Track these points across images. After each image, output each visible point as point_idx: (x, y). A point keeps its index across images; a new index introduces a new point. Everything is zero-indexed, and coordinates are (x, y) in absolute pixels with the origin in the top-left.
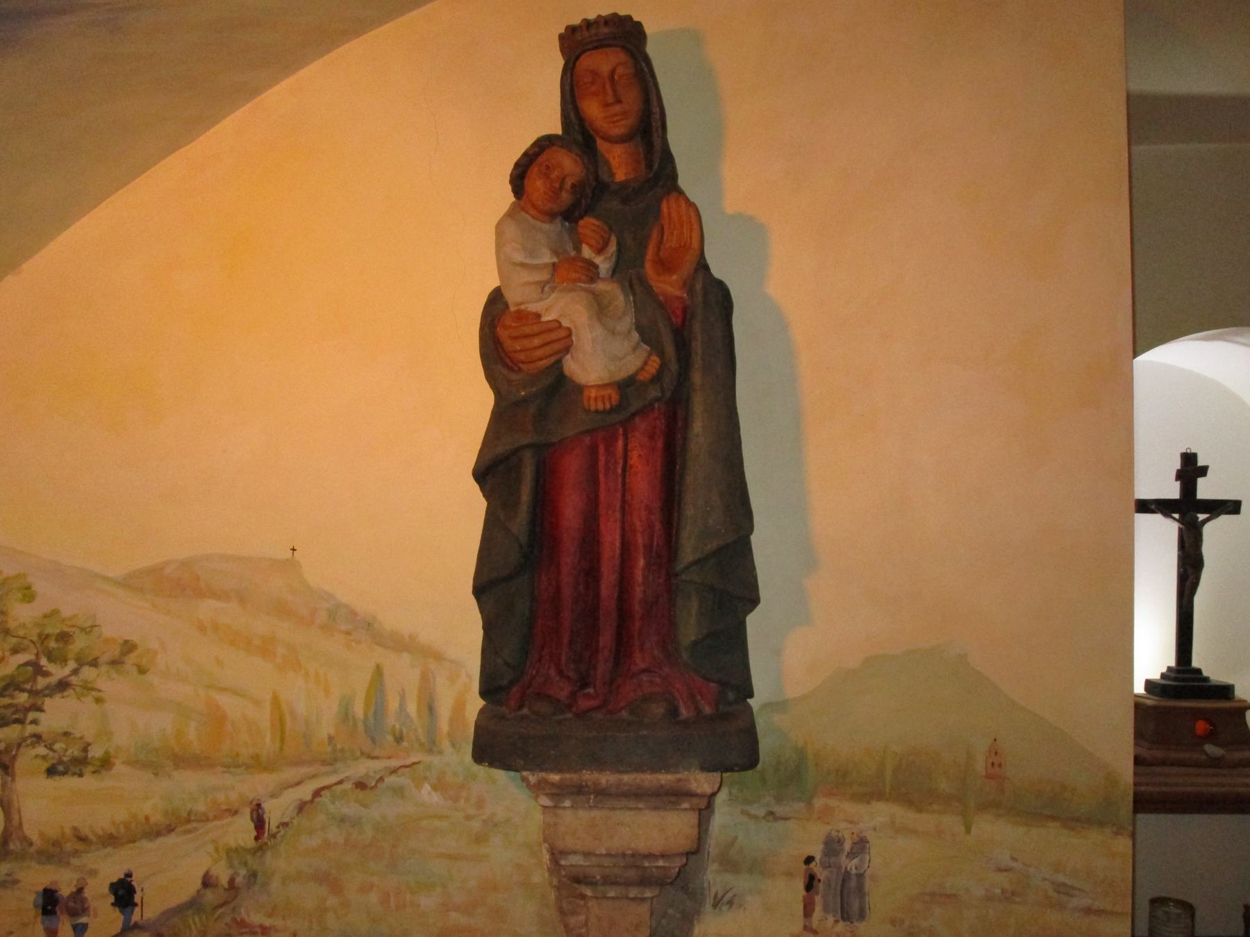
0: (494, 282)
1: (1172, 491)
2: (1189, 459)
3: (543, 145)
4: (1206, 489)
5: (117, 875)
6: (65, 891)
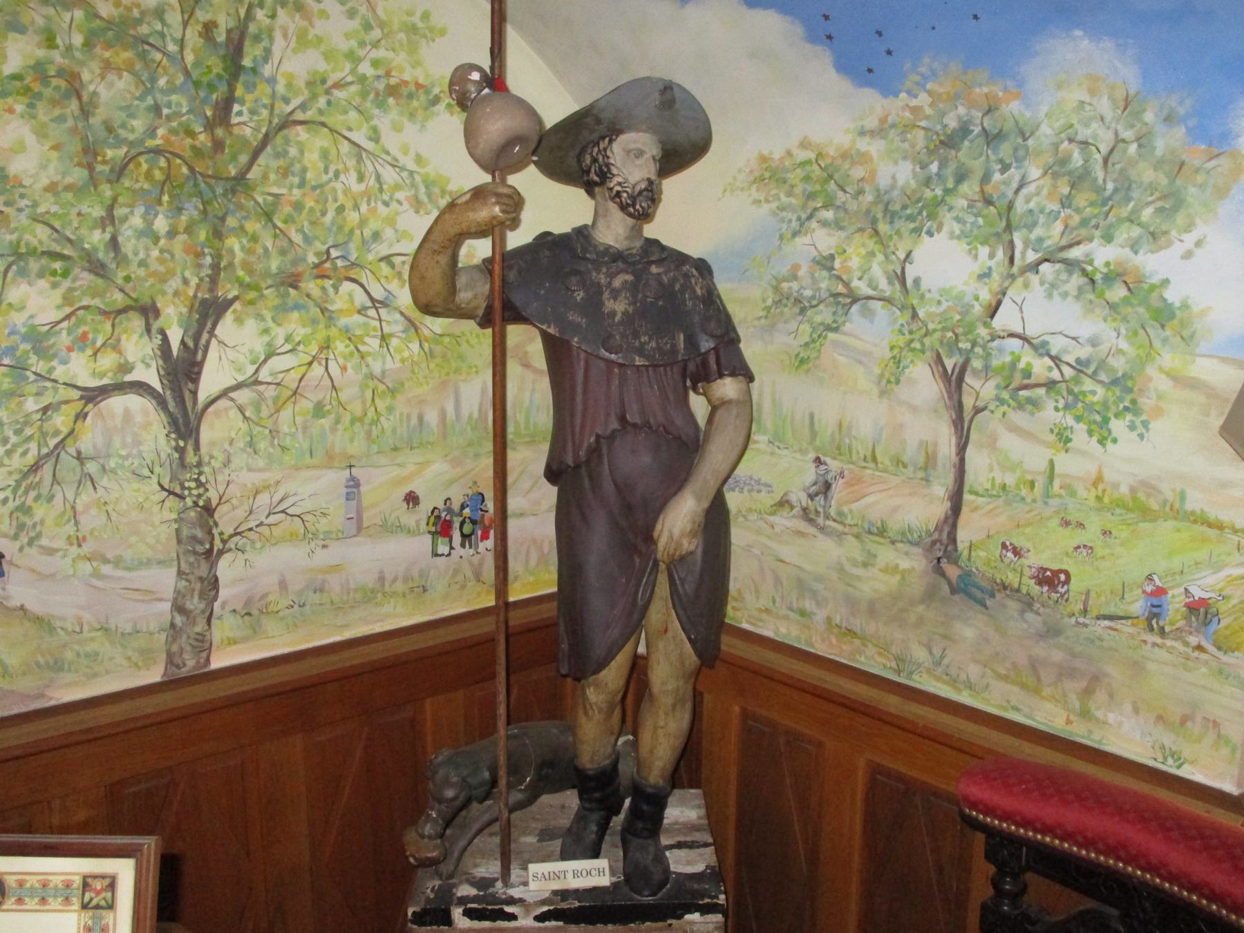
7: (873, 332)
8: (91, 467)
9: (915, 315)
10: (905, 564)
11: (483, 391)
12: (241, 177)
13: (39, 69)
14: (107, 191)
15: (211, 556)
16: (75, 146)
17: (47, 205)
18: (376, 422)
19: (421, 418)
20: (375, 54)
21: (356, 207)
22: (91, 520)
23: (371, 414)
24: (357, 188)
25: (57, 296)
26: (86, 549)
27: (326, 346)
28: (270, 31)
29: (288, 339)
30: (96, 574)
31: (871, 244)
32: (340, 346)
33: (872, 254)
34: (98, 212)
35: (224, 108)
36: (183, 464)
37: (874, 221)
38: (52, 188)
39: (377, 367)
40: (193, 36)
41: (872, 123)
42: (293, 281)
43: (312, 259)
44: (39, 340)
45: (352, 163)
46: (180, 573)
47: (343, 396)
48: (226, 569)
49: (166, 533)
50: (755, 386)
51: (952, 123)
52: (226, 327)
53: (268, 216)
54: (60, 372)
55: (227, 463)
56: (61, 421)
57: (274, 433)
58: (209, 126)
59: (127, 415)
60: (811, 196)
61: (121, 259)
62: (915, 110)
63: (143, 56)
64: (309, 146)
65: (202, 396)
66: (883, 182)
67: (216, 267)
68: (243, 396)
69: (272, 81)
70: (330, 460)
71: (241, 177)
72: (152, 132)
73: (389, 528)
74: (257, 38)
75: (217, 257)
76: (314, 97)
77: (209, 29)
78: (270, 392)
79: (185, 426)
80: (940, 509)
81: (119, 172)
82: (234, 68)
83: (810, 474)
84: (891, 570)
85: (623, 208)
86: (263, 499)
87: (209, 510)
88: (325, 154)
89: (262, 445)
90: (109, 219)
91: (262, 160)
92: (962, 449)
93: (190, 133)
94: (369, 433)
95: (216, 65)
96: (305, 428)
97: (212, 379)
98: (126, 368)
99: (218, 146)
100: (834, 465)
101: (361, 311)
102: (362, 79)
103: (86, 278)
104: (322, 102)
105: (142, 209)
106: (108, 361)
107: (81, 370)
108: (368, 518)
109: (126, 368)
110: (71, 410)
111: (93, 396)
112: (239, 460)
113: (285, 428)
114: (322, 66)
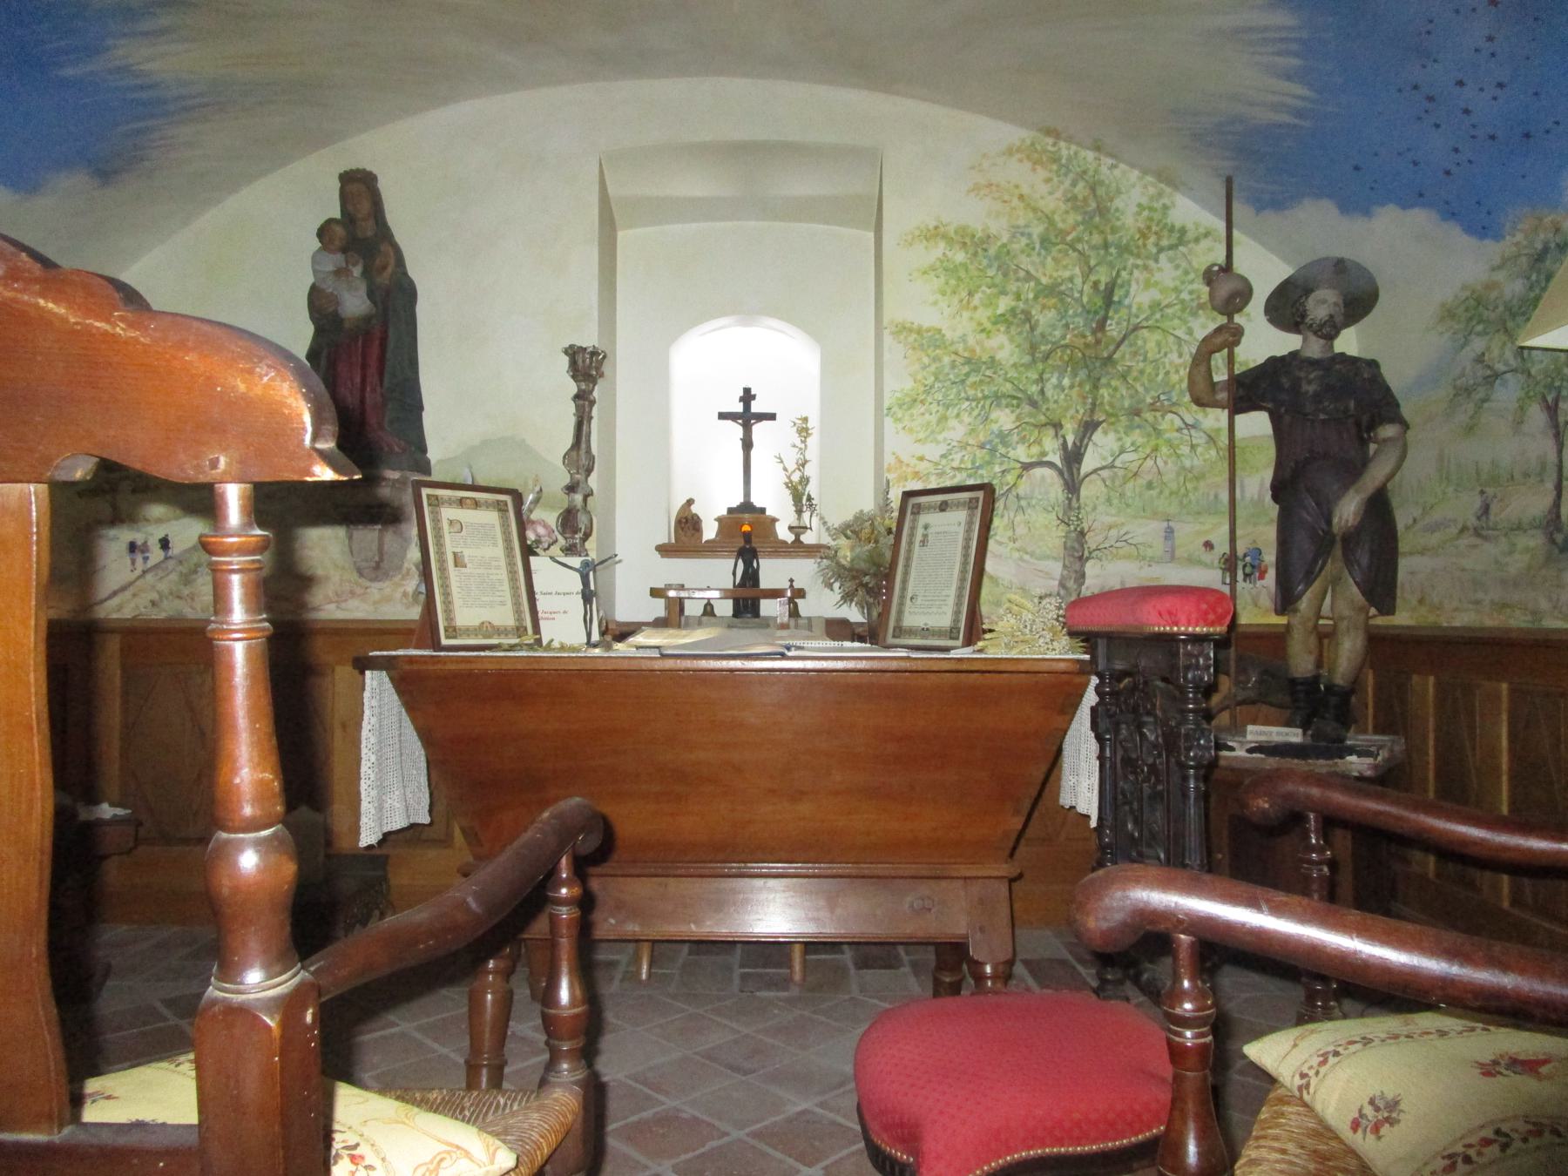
0: (310, 280)
1: (739, 408)
2: (747, 391)
3: (330, 221)
4: (756, 407)
5: (161, 535)
6: (139, 543)
7: (1507, 394)
8: (1023, 503)
9: (1529, 375)
10: (1532, 544)
11: (1262, 485)
12: (1110, 358)
13: (1013, 311)
14: (1040, 366)
15: (1082, 560)
16: (1027, 345)
17: (1012, 374)
18: (1186, 495)
19: (1216, 496)
20: (1190, 287)
21: (1177, 372)
22: (1021, 530)
23: (1183, 490)
24: (1178, 361)
25: (1013, 417)
26: (1017, 545)
27: (1156, 449)
28: (1129, 283)
29: (1133, 444)
30: (1021, 559)
31: (1504, 338)
32: (1164, 450)
33: (1504, 344)
34: (1035, 376)
35: (1101, 325)
36: (1070, 507)
37: (1505, 322)
38: (1014, 365)
39: (1187, 463)
40: (1087, 288)
41: (1497, 261)
42: (1137, 413)
43: (1149, 400)
44: (1003, 437)
45: (1175, 348)
46: (1065, 566)
47: (1165, 479)
48: (1091, 568)
49: (1059, 543)
50: (1409, 433)
51: (1539, 246)
52: (1098, 436)
53: (1124, 377)
54: (1012, 454)
55: (1095, 508)
56: (1010, 478)
57: (1122, 495)
58: (1094, 332)
59: (1043, 478)
60: (1471, 319)
61: (1046, 400)
62: (1517, 244)
63: (1062, 300)
64: (1149, 340)
65: (1083, 472)
66: (1508, 295)
67: (1094, 404)
68: (1105, 473)
69: (1130, 307)
70: (1155, 515)
71: (1110, 358)
72: (1064, 337)
73: (1191, 561)
74: (1122, 286)
75: (1095, 399)
76: (1153, 314)
77: (1096, 284)
78: (1121, 473)
79: (1072, 486)
80: (1549, 500)
81: (1047, 357)
82: (1108, 301)
83: (1477, 503)
84: (1527, 550)
85: (1315, 333)
86: (1113, 532)
87: (1082, 534)
88: (1159, 344)
89: (1115, 502)
90: (1041, 379)
91: (1122, 348)
92: (1560, 452)
93: (1084, 337)
94: (1181, 502)
95: (1099, 302)
96: (1141, 495)
97: (1089, 462)
98: (1044, 454)
99: (1098, 342)
100: (1490, 491)
101: (1179, 430)
102: (1182, 302)
103: (1027, 408)
104: (1158, 316)
105: (999, 228)
106: (1035, 450)
107: (1022, 453)
108: (1178, 553)
109: (1044, 454)
110: (1016, 473)
111: (1027, 467)
112: (1101, 508)
113: (1129, 494)
114: (1158, 296)
